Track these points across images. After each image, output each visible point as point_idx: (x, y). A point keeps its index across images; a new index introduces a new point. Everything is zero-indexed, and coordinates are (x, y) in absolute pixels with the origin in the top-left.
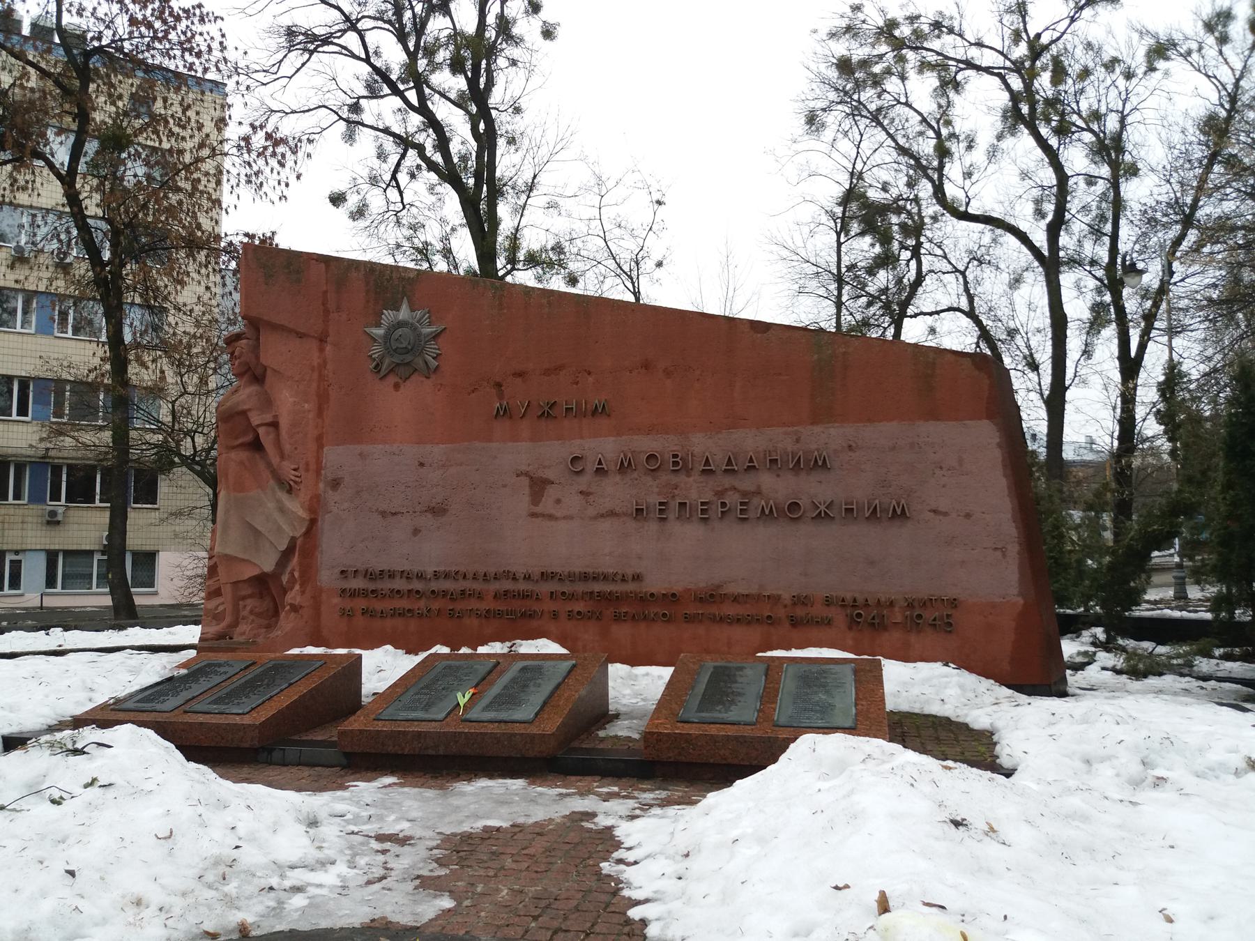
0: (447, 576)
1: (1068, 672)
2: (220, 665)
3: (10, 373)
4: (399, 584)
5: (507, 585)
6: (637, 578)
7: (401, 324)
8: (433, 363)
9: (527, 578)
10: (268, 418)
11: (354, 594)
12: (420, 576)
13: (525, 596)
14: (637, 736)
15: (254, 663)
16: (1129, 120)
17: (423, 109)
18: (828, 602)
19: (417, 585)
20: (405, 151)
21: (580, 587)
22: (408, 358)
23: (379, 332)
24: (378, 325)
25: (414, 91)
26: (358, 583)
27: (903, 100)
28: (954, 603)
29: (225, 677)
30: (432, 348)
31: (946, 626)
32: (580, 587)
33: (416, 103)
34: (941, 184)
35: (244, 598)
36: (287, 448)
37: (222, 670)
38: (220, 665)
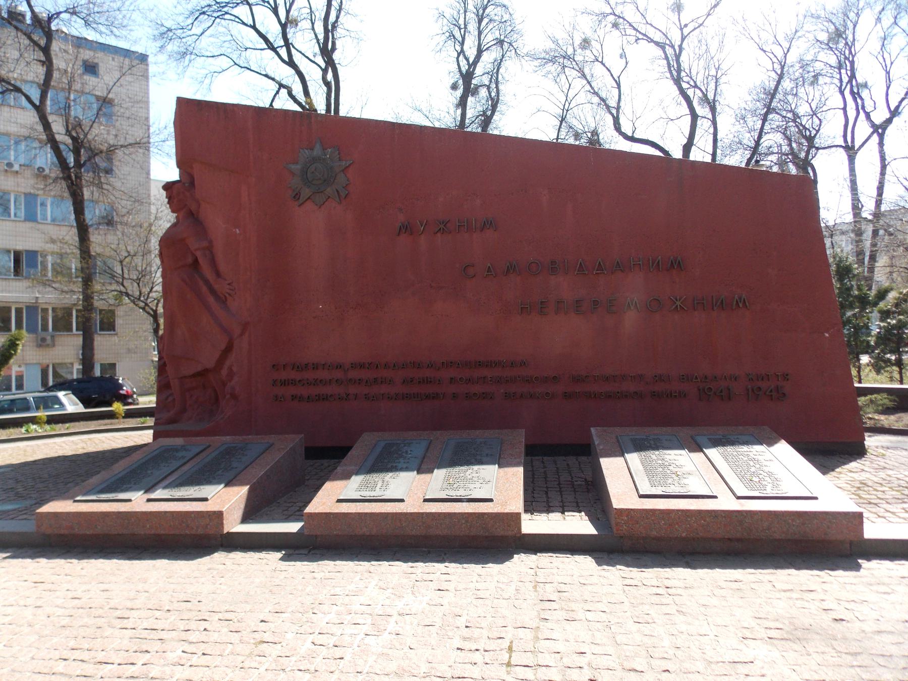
0: (362, 366)
1: (866, 434)
2: (177, 450)
3: (34, 249)
6: (523, 364)
7: (314, 160)
9: (430, 366)
11: (285, 383)
12: (339, 367)
14: (583, 513)
15: (209, 446)
16: (721, 81)
17: (291, 63)
19: (338, 374)
20: (279, 89)
23: (296, 168)
25: (284, 48)
26: (284, 375)
27: (600, 60)
28: (785, 377)
29: (182, 461)
30: (341, 179)
33: (286, 59)
34: (618, 116)
36: (222, 267)
37: (180, 454)
38: (177, 450)
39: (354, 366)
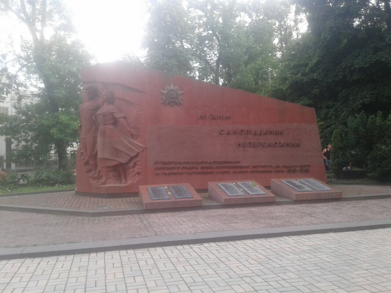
4: (172, 166)
5: (204, 165)
6: (239, 162)
7: (172, 90)
8: (182, 102)
10: (123, 115)
11: (160, 169)
12: (179, 163)
13: (210, 168)
18: (284, 166)
19: (178, 166)
21: (224, 165)
22: (174, 100)
24: (164, 90)
26: (159, 166)
31: (307, 171)
32: (224, 165)
35: (109, 172)
39: (184, 163)
